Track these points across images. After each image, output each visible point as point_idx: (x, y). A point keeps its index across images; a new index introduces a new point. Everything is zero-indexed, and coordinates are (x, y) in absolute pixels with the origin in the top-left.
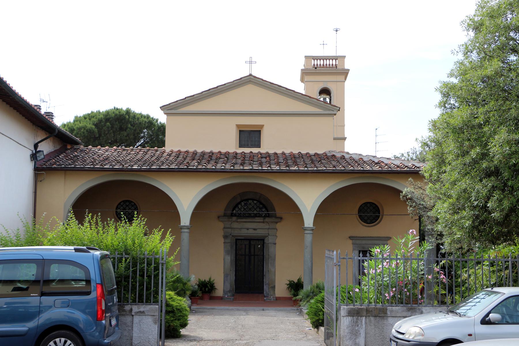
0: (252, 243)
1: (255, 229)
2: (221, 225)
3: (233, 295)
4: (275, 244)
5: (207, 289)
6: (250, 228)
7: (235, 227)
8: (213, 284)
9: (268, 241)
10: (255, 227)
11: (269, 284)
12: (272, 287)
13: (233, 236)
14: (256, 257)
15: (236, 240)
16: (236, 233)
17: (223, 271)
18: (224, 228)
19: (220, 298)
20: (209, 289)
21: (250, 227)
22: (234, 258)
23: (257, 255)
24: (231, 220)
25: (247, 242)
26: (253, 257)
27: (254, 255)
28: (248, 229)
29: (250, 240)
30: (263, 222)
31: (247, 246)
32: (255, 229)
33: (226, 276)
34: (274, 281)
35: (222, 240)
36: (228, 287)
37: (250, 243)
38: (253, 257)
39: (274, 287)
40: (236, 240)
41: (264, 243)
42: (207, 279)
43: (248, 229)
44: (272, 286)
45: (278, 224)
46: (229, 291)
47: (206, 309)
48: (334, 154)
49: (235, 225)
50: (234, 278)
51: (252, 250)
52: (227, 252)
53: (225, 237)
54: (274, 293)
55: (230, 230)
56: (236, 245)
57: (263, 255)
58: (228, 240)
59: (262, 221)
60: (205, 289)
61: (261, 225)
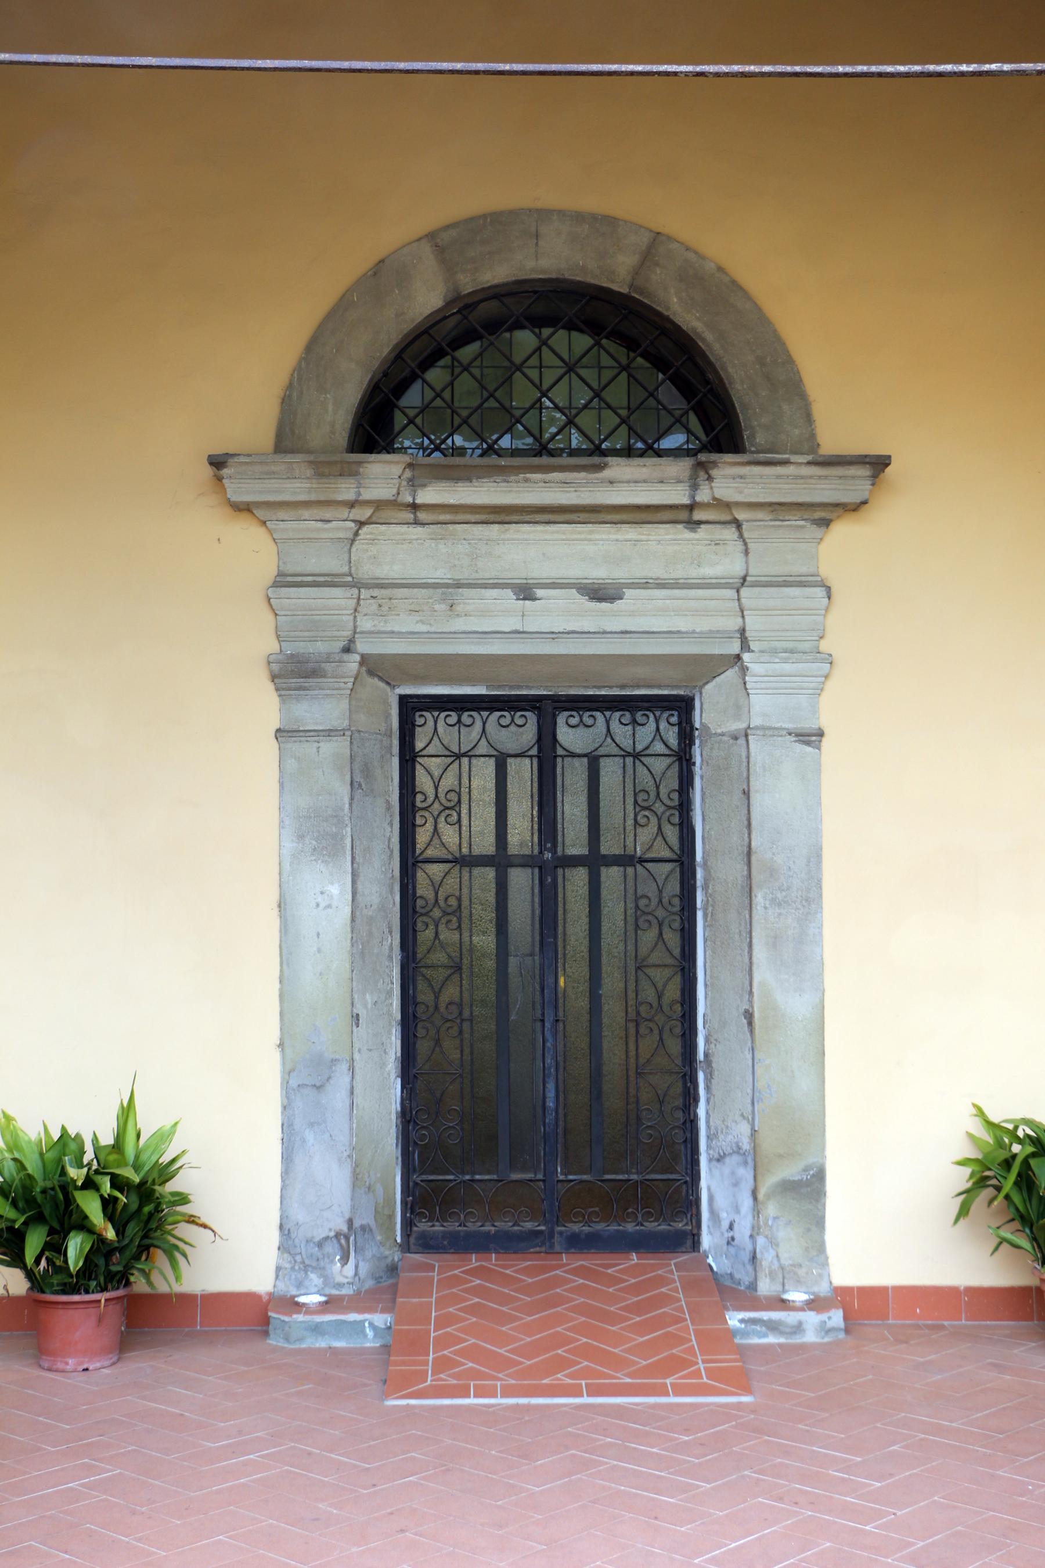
0: (570, 735)
1: (600, 593)
2: (250, 552)
3: (386, 1289)
4: (812, 737)
5: (76, 1247)
6: (552, 570)
7: (390, 570)
8: (166, 1172)
9: (740, 709)
10: (599, 573)
11: (754, 1158)
12: (789, 1187)
13: (372, 666)
14: (611, 876)
15: (410, 707)
16: (404, 631)
17: (274, 1033)
18: (283, 581)
19: (250, 1316)
20: (100, 1248)
21: (540, 571)
22: (382, 891)
23: (626, 860)
24: (346, 490)
25: (523, 733)
26: (577, 879)
27: (594, 861)
28: (526, 592)
29: (543, 707)
30: (686, 515)
31: (522, 775)
32: (600, 593)
33: (306, 1079)
34: (809, 1128)
35: (266, 709)
36: (332, 1197)
37: (547, 755)
38: (577, 879)
39: (809, 1190)
40: (410, 707)
41: (687, 734)
42: (96, 1127)
43: (526, 592)
44: (791, 1171)
45: (842, 530)
46: (346, 1241)
47: (866, 1325)
48: (692, 535)
49: (399, 552)
50: (384, 1094)
51: (572, 809)
52: (315, 834)
53: (294, 674)
54: (818, 1250)
55: (340, 599)
56: (408, 758)
57: (685, 860)
58: (325, 709)
59: (678, 495)
60: (55, 1247)
61: (661, 548)
